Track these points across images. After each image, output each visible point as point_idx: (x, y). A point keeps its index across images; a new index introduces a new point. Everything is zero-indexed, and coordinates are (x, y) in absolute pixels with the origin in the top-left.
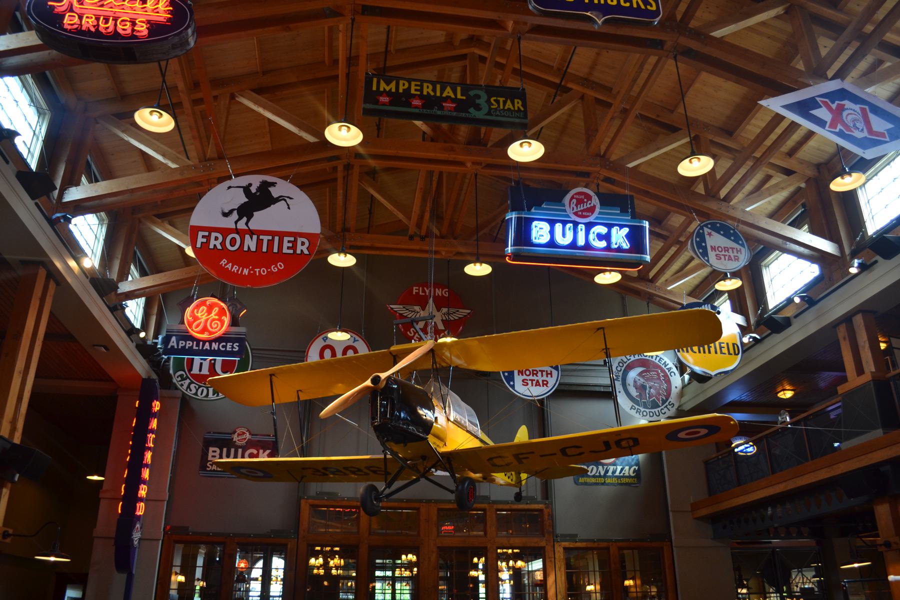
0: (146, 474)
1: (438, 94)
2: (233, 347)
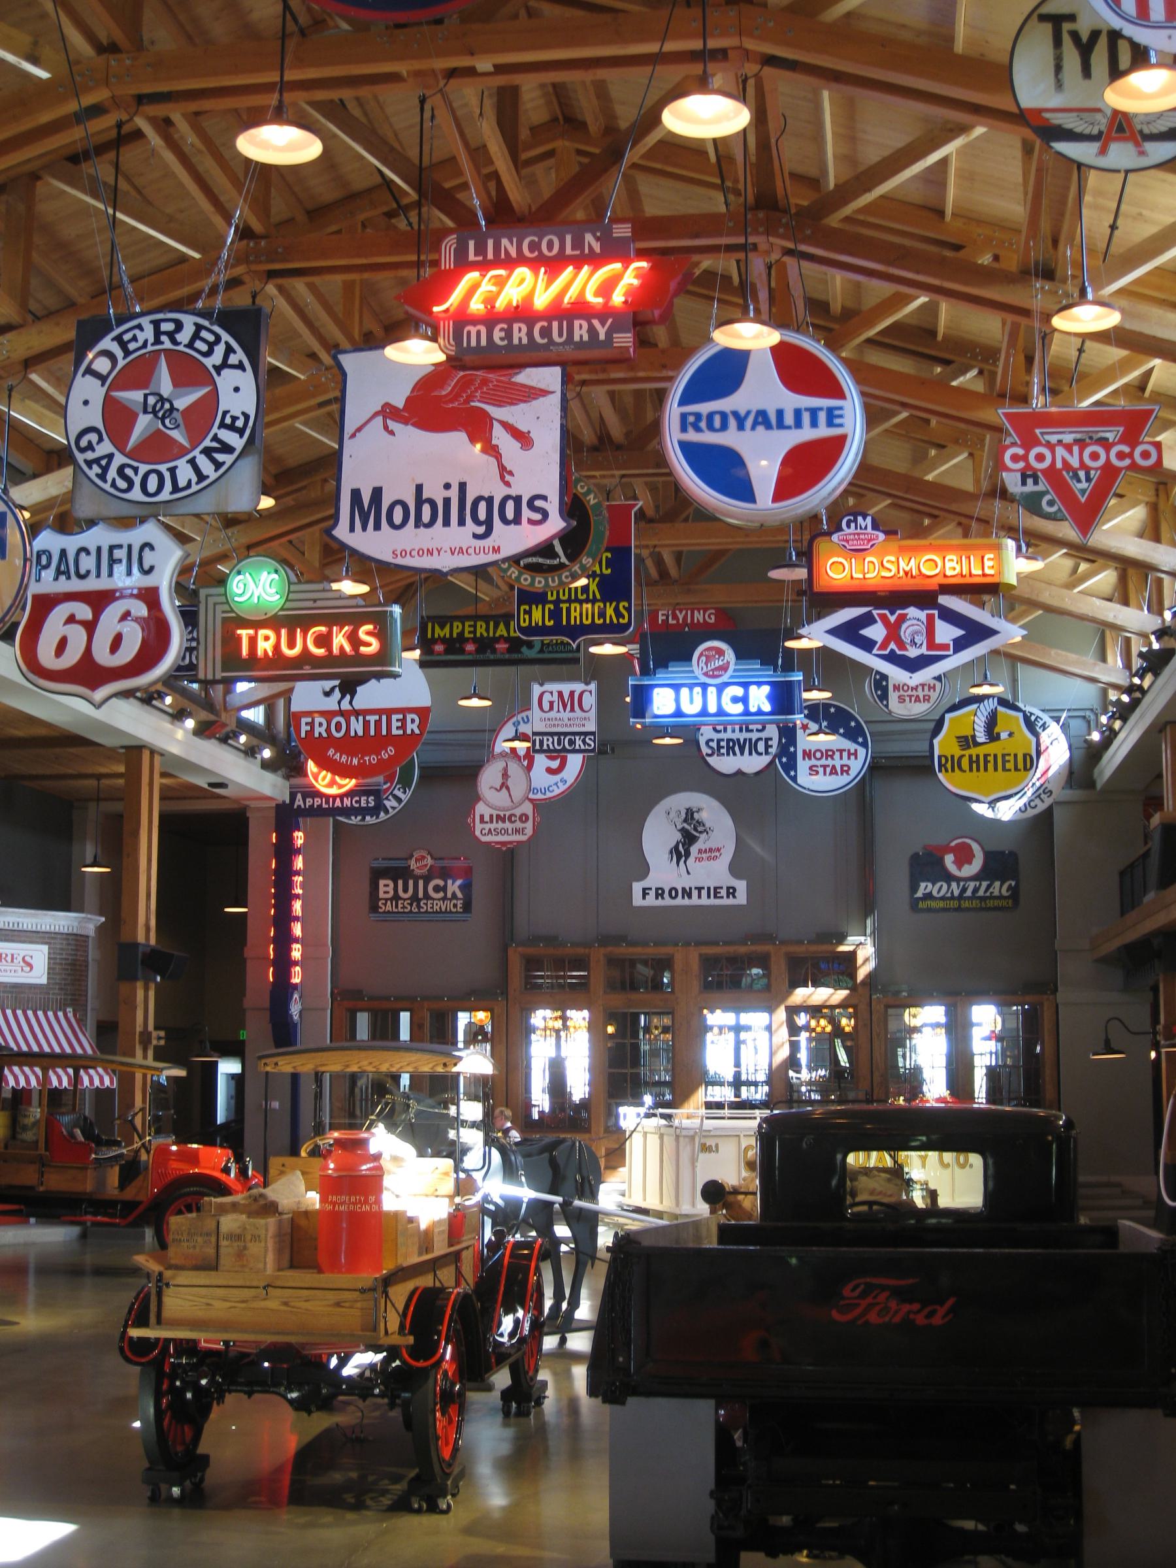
0: (297, 930)
1: (491, 634)
2: (368, 802)
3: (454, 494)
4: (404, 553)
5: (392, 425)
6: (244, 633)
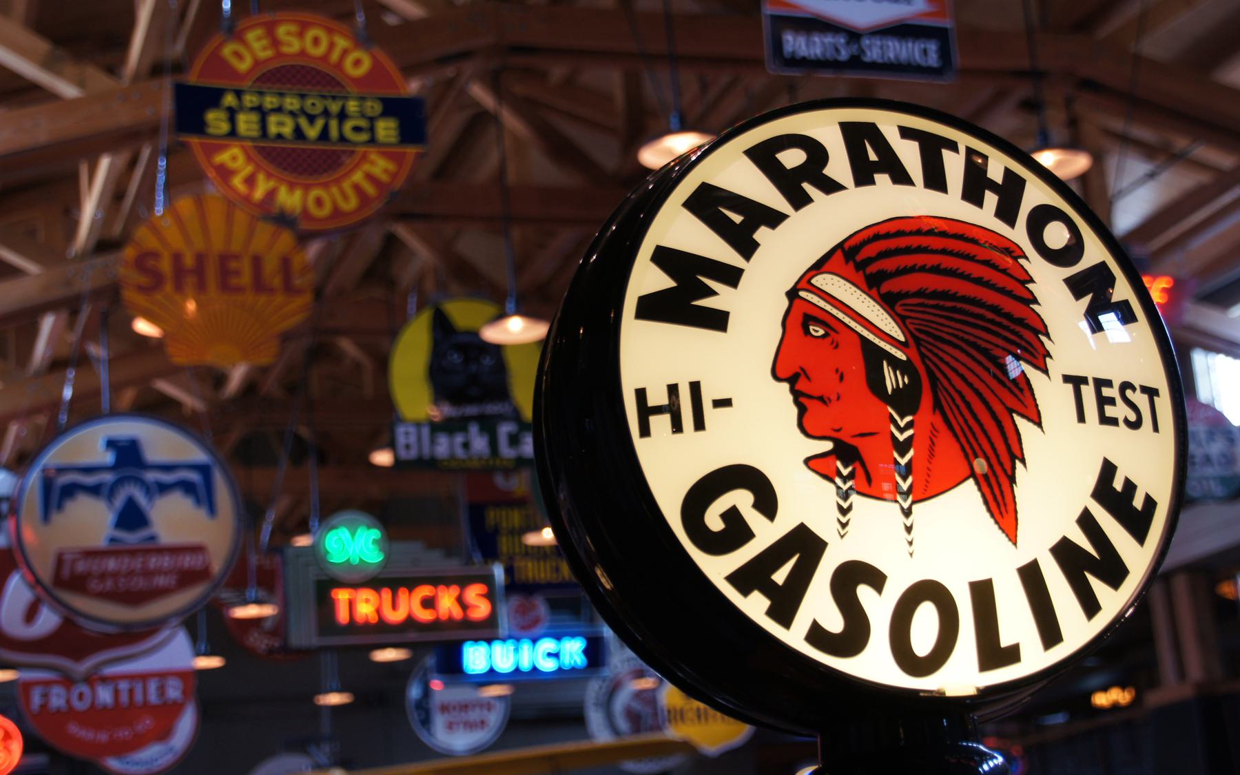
6: (342, 596)
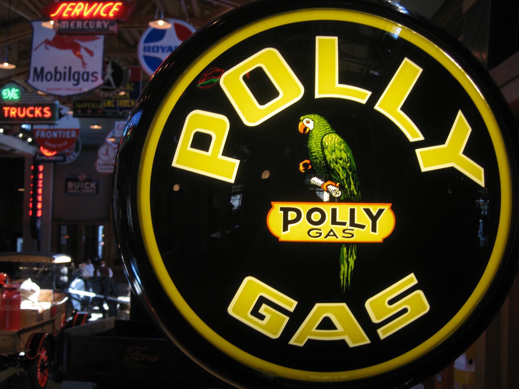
3: (67, 70)
4: (50, 89)
5: (49, 47)
6: (6, 109)
